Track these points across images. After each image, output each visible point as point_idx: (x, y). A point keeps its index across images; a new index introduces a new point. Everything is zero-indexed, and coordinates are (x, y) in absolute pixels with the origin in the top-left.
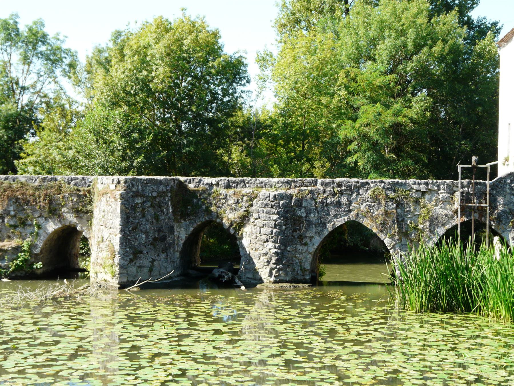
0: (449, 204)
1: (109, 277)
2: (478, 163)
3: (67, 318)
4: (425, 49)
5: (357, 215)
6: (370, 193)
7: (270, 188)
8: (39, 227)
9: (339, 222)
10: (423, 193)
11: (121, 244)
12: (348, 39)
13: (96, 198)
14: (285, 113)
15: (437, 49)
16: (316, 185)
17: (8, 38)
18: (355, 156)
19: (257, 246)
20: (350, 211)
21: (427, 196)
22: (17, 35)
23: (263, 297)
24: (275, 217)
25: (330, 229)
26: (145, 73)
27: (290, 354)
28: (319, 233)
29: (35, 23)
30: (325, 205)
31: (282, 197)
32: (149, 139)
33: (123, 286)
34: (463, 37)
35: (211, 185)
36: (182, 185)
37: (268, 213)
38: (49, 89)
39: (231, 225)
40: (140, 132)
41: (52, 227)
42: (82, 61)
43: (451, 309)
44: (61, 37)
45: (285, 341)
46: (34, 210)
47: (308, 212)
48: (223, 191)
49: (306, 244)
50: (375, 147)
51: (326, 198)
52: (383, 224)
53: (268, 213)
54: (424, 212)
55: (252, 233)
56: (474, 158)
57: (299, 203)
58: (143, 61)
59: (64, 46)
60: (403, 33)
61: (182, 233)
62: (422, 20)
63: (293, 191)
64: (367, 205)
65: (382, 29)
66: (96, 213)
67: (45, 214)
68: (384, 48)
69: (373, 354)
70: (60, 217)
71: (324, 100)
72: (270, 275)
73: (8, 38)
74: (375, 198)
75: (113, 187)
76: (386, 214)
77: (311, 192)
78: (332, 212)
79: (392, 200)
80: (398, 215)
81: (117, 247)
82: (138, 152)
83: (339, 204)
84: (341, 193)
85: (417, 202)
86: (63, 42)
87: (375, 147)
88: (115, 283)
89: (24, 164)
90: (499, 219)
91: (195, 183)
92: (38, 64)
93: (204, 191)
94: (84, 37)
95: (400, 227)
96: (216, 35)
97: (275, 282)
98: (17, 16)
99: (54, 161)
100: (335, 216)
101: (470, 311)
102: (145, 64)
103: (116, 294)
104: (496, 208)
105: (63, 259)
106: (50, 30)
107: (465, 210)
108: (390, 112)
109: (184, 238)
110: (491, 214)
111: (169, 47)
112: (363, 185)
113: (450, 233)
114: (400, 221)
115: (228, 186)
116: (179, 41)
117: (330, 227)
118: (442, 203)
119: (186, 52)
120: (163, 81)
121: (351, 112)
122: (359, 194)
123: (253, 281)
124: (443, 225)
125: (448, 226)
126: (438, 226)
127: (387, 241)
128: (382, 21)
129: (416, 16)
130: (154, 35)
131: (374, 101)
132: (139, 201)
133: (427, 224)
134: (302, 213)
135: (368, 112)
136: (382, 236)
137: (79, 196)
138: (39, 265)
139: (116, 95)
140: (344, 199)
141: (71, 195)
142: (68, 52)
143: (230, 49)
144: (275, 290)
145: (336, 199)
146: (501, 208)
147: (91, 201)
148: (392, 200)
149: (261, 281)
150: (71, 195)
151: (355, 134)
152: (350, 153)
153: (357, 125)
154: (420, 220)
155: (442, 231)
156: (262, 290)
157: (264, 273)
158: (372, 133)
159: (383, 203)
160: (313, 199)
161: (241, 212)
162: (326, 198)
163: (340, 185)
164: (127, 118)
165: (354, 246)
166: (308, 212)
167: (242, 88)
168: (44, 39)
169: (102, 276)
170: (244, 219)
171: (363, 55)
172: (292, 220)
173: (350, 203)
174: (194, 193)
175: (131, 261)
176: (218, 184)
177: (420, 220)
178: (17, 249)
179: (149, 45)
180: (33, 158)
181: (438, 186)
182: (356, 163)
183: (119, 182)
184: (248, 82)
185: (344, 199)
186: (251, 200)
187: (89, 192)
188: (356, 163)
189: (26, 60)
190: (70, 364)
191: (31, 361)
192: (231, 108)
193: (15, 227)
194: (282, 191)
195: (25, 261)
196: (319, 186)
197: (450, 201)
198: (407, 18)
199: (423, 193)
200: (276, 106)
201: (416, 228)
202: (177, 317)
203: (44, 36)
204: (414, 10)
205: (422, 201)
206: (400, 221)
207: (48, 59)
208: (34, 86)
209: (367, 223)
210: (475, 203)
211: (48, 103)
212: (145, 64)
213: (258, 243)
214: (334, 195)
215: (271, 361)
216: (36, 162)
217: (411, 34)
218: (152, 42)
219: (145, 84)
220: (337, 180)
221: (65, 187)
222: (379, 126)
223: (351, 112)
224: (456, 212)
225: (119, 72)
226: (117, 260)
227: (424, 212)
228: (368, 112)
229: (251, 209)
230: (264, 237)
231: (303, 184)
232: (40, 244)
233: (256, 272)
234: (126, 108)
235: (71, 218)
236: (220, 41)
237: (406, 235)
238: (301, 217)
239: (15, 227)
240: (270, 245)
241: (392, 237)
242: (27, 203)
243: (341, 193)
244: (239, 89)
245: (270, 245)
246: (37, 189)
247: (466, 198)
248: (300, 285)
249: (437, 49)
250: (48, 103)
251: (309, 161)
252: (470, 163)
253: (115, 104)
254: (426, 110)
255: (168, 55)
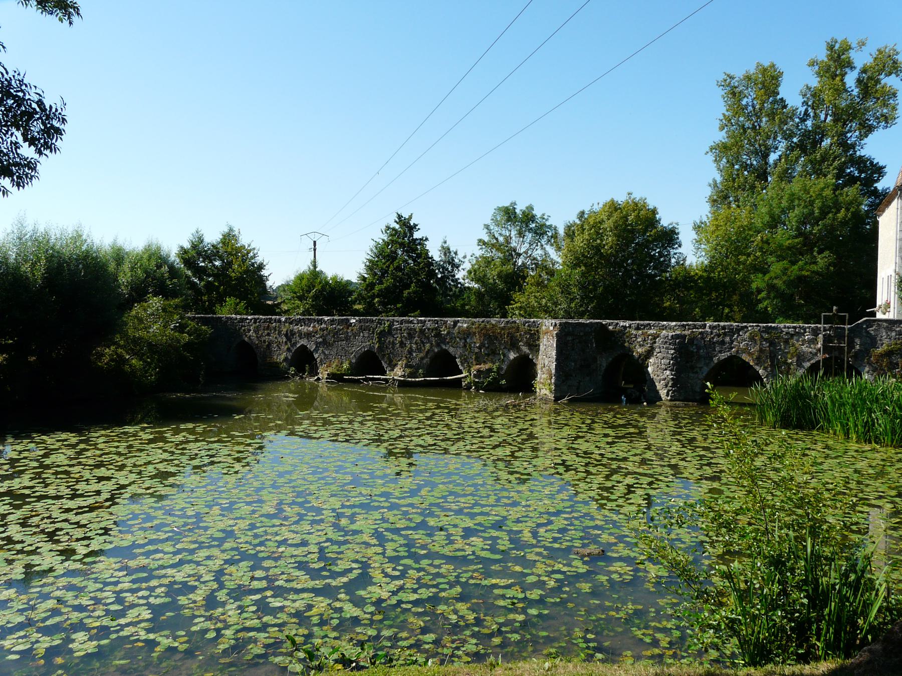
0: (814, 343)
1: (547, 392)
2: (838, 311)
3: (507, 420)
4: (830, 215)
5: (737, 351)
6: (747, 334)
7: (670, 329)
8: (504, 356)
9: (723, 356)
10: (792, 335)
11: (556, 369)
12: (764, 210)
13: (541, 336)
14: (709, 269)
15: (841, 215)
16: (705, 328)
17: (509, 220)
18: (765, 303)
19: (658, 373)
20: (732, 348)
21: (795, 338)
22: (515, 217)
23: (662, 413)
24: (673, 351)
25: (716, 361)
26: (599, 241)
27: (649, 455)
28: (707, 365)
29: (527, 208)
30: (712, 344)
31: (677, 336)
32: (600, 290)
33: (557, 399)
34: (529, 288)
35: (625, 327)
36: (604, 327)
37: (667, 348)
38: (538, 253)
39: (640, 356)
40: (594, 285)
41: (512, 356)
42: (561, 231)
43: (800, 427)
44: (546, 217)
45: (651, 444)
46: (500, 344)
47: (699, 348)
48: (634, 332)
49: (697, 372)
50: (780, 295)
51: (713, 338)
52: (758, 358)
53: (667, 348)
54: (792, 349)
55: (655, 363)
56: (835, 308)
57: (692, 340)
58: (598, 233)
59: (548, 223)
60: (812, 203)
61: (604, 362)
62: (828, 192)
63: (686, 333)
64: (745, 342)
65: (792, 201)
66: (542, 348)
67: (508, 347)
68: (794, 215)
69: (712, 458)
70: (518, 349)
71: (742, 258)
72: (667, 395)
73: (509, 220)
74: (752, 338)
75: (551, 328)
76: (761, 351)
77: (701, 333)
78: (717, 349)
79: (766, 340)
80: (771, 352)
81: (553, 371)
82: (591, 300)
83: (723, 343)
84: (725, 334)
85: (786, 342)
86: (547, 220)
87: (780, 295)
88: (551, 397)
89: (513, 309)
90: (856, 356)
91: (612, 324)
92: (529, 236)
93: (620, 331)
94: (560, 215)
95: (772, 362)
96: (654, 212)
97: (670, 400)
98: (515, 204)
99: (533, 307)
100: (720, 352)
101: (814, 428)
102: (599, 234)
103: (551, 405)
104: (854, 347)
105: (520, 379)
106: (537, 212)
107: (826, 348)
108: (796, 267)
109: (605, 365)
110: (849, 352)
111: (616, 222)
112: (743, 328)
113: (814, 369)
114: (773, 356)
115: (638, 328)
116: (625, 218)
117: (715, 360)
118: (809, 341)
119: (631, 225)
120: (611, 247)
121: (761, 268)
122: (739, 335)
123: (654, 398)
124: (809, 361)
125: (813, 361)
126: (804, 361)
127: (761, 372)
128: (793, 195)
129: (822, 189)
130: (607, 214)
131: (780, 258)
132: (570, 338)
133: (795, 359)
134: (694, 349)
135: (776, 268)
136: (757, 368)
137: (531, 334)
138: (504, 382)
139: (577, 258)
140: (727, 339)
141: (525, 333)
142: (550, 227)
143: (665, 220)
144: (670, 407)
145: (721, 339)
146: (858, 347)
147: (539, 338)
148: (766, 340)
149: (660, 399)
150: (525, 333)
151: (764, 285)
152: (760, 301)
153: (767, 277)
154: (789, 356)
155: (807, 365)
156: (660, 406)
157: (663, 393)
158: (778, 283)
159: (758, 342)
160: (703, 338)
161: (647, 347)
162: (713, 338)
163: (724, 328)
164: (583, 274)
165: (737, 375)
166: (699, 348)
167: (675, 251)
168: (532, 218)
169: (544, 392)
170: (649, 353)
171: (774, 222)
172: (686, 355)
173: (732, 341)
174: (612, 333)
175: (563, 381)
176: (630, 327)
177: (789, 356)
178: (490, 370)
179: (603, 221)
180: (518, 305)
181: (805, 330)
182: (766, 308)
183: (556, 325)
184: (680, 246)
185: (727, 339)
186: (655, 338)
187: (538, 331)
188: (766, 308)
189: (521, 234)
190: (491, 451)
191: (468, 448)
192: (662, 265)
193: (488, 355)
194: (678, 332)
195: (494, 379)
196: (707, 329)
197: (814, 341)
198: (814, 192)
199: (792, 335)
200: (690, 266)
201: (785, 363)
202: (583, 423)
203: (534, 216)
204: (822, 185)
205: (791, 341)
206: (773, 356)
207: (536, 233)
208: (526, 252)
209: (745, 357)
210: (835, 343)
211: (536, 264)
212: (599, 234)
213: (659, 370)
214: (719, 335)
215: (631, 459)
216: (521, 307)
217: (818, 203)
218: (605, 218)
219: (598, 249)
220: (722, 324)
221: (522, 327)
222: (785, 278)
223: (761, 268)
224: (819, 350)
225: (580, 242)
226: (553, 381)
227: (792, 349)
228: (776, 268)
229: (655, 345)
230: (663, 366)
231: (695, 327)
232: (504, 367)
233: (657, 392)
234: (583, 268)
235: (525, 349)
236: (657, 216)
237: (778, 366)
238: (692, 352)
239: (488, 355)
240: (668, 372)
241: (765, 369)
242: (496, 338)
243: (725, 334)
244: (672, 251)
245: (668, 372)
246: (503, 329)
247: (827, 339)
248: (690, 403)
249: (841, 215)
250: (536, 264)
251: (729, 306)
252: (831, 311)
253: (575, 266)
254: (830, 265)
255: (616, 228)
